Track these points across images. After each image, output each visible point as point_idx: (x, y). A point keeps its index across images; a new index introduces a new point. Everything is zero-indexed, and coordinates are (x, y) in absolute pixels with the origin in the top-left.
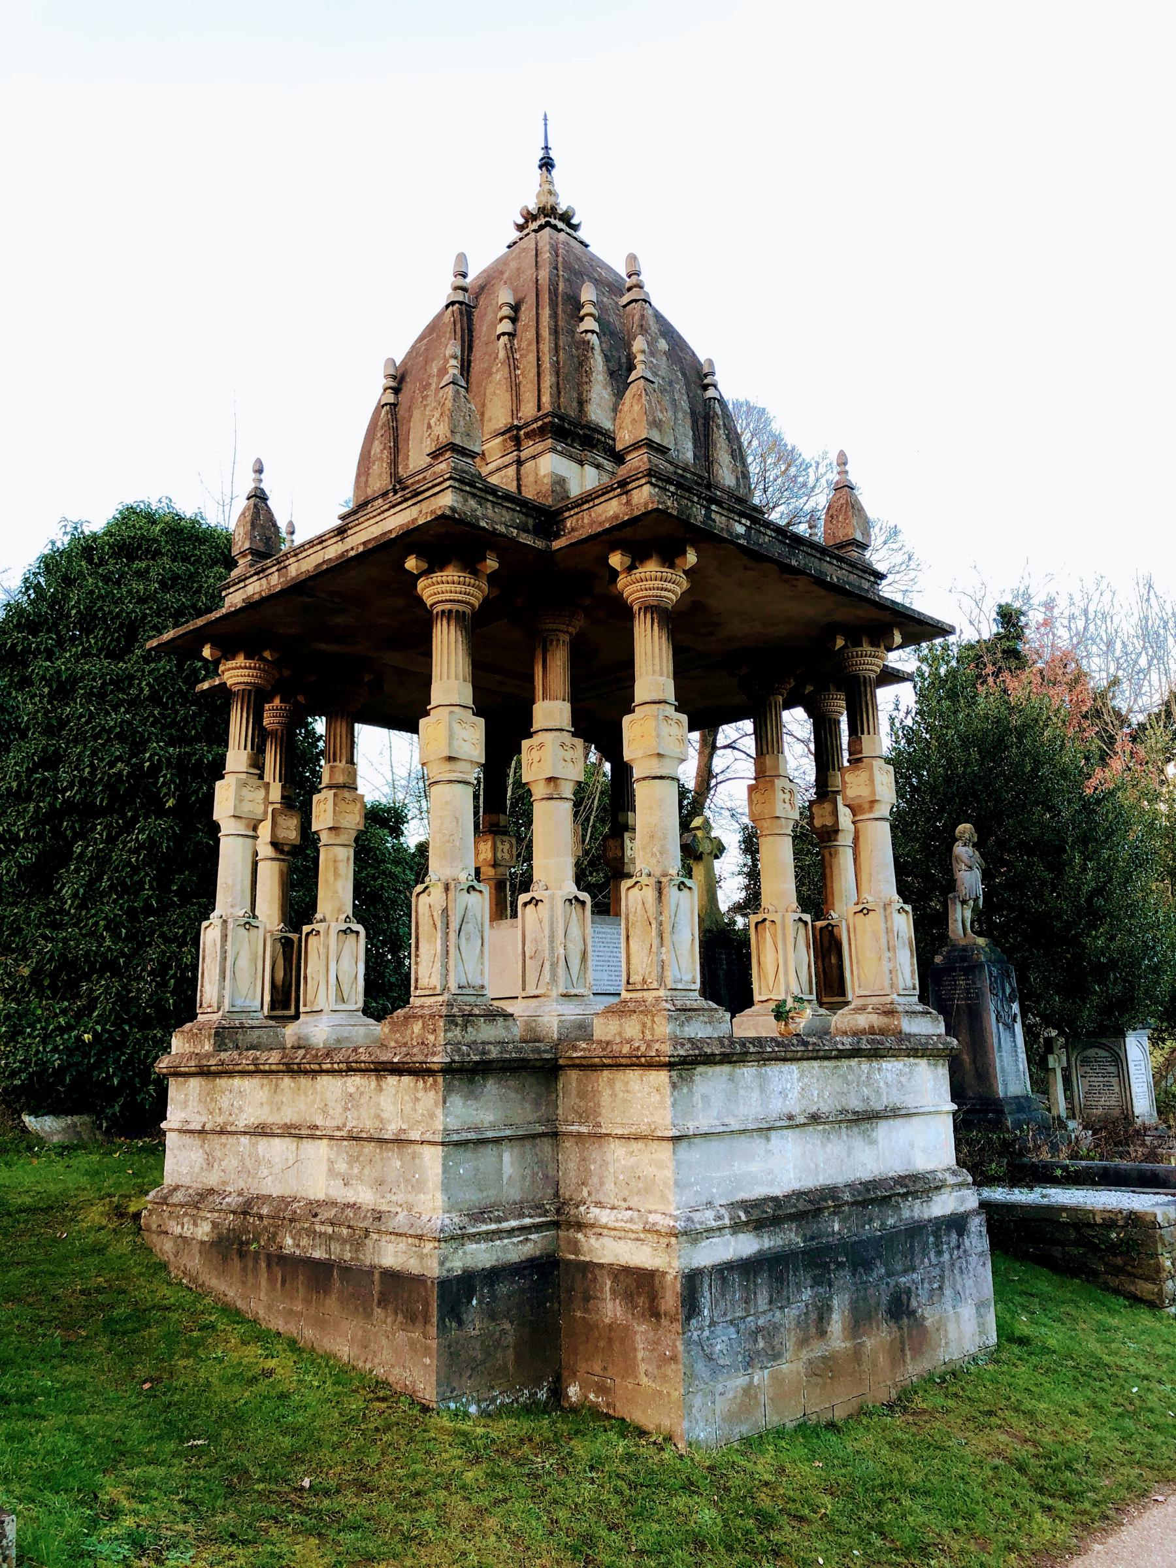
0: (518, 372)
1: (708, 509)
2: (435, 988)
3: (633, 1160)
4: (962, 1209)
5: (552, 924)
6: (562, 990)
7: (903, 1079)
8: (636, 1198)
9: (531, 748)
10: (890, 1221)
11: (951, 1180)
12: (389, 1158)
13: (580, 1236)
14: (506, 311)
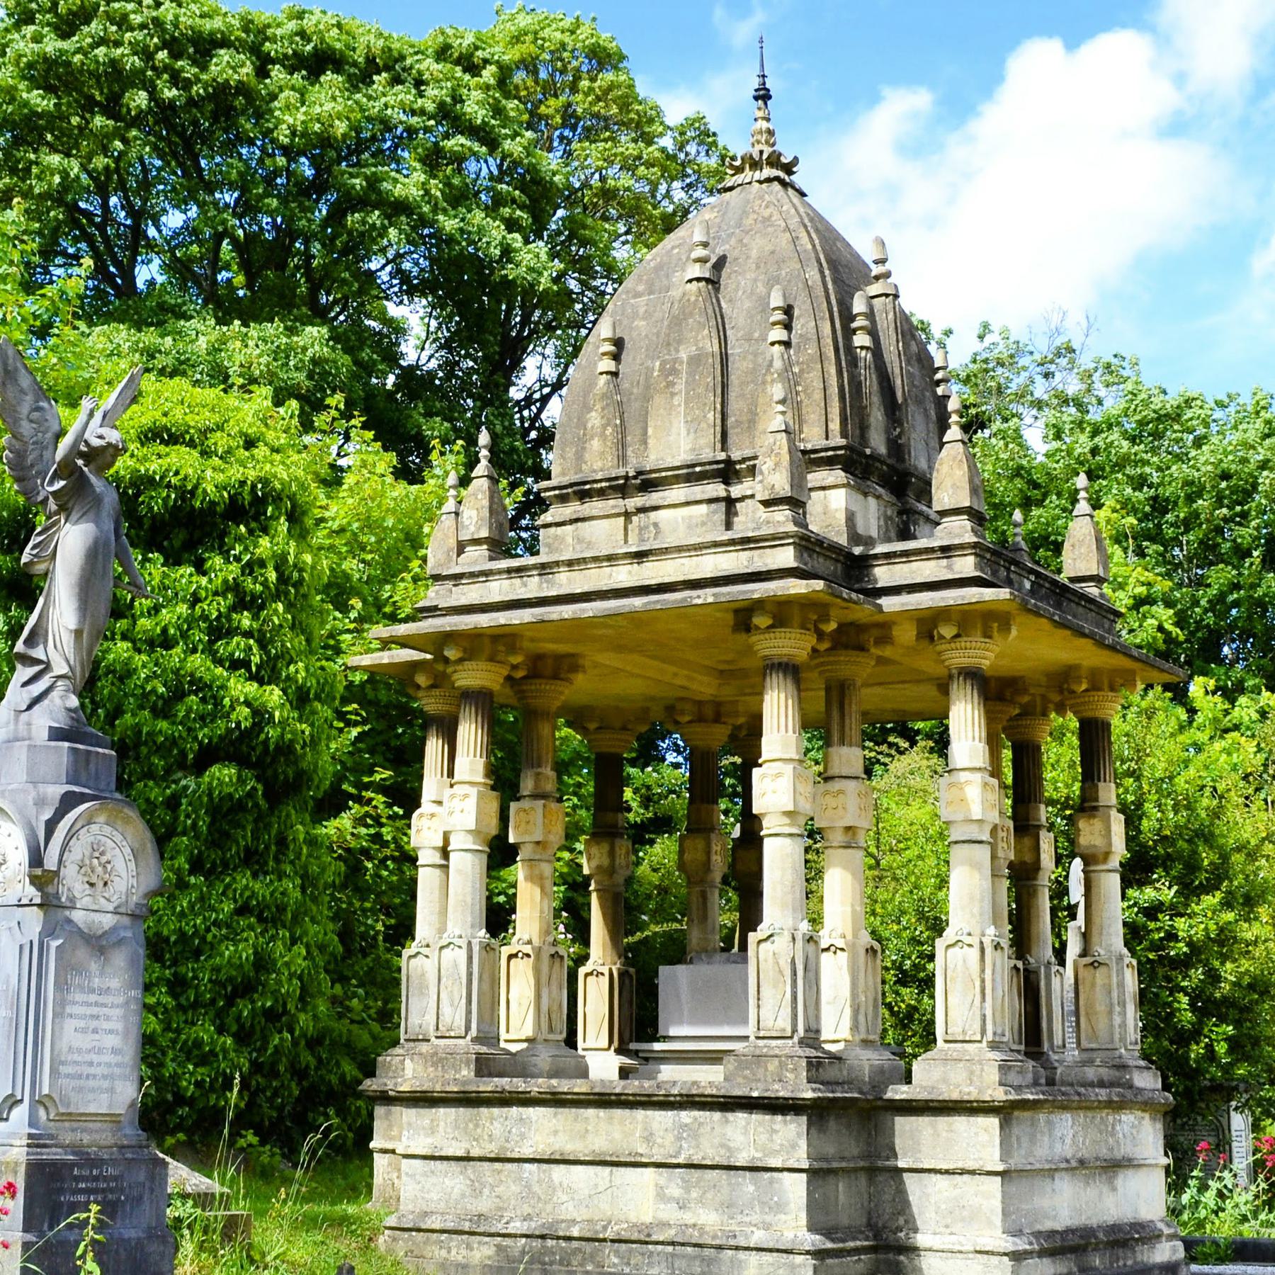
0: (800, 388)
1: (1008, 570)
2: (784, 1030)
3: (958, 1191)
4: (1174, 1258)
5: (444, 912)
6: (863, 1036)
7: (1134, 1132)
8: (960, 1225)
9: (764, 776)
10: (1130, 1263)
11: (1167, 1231)
12: (739, 1184)
13: (902, 1258)
14: (778, 316)
